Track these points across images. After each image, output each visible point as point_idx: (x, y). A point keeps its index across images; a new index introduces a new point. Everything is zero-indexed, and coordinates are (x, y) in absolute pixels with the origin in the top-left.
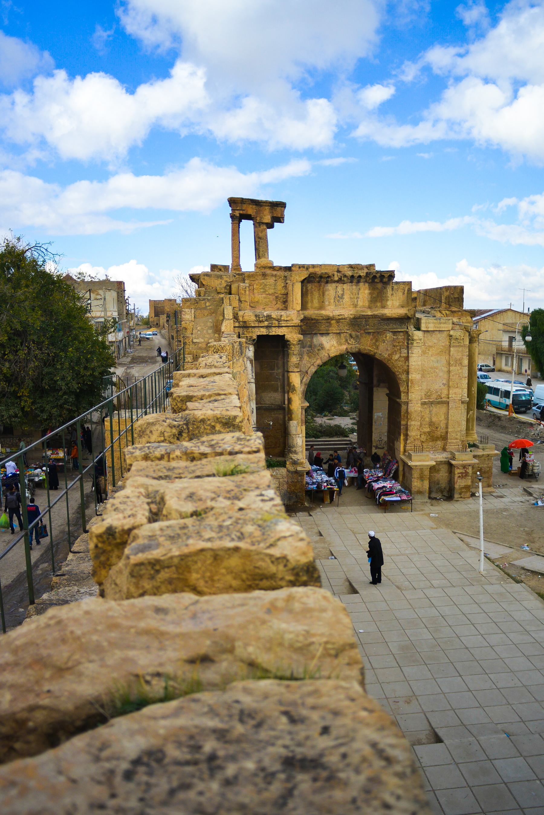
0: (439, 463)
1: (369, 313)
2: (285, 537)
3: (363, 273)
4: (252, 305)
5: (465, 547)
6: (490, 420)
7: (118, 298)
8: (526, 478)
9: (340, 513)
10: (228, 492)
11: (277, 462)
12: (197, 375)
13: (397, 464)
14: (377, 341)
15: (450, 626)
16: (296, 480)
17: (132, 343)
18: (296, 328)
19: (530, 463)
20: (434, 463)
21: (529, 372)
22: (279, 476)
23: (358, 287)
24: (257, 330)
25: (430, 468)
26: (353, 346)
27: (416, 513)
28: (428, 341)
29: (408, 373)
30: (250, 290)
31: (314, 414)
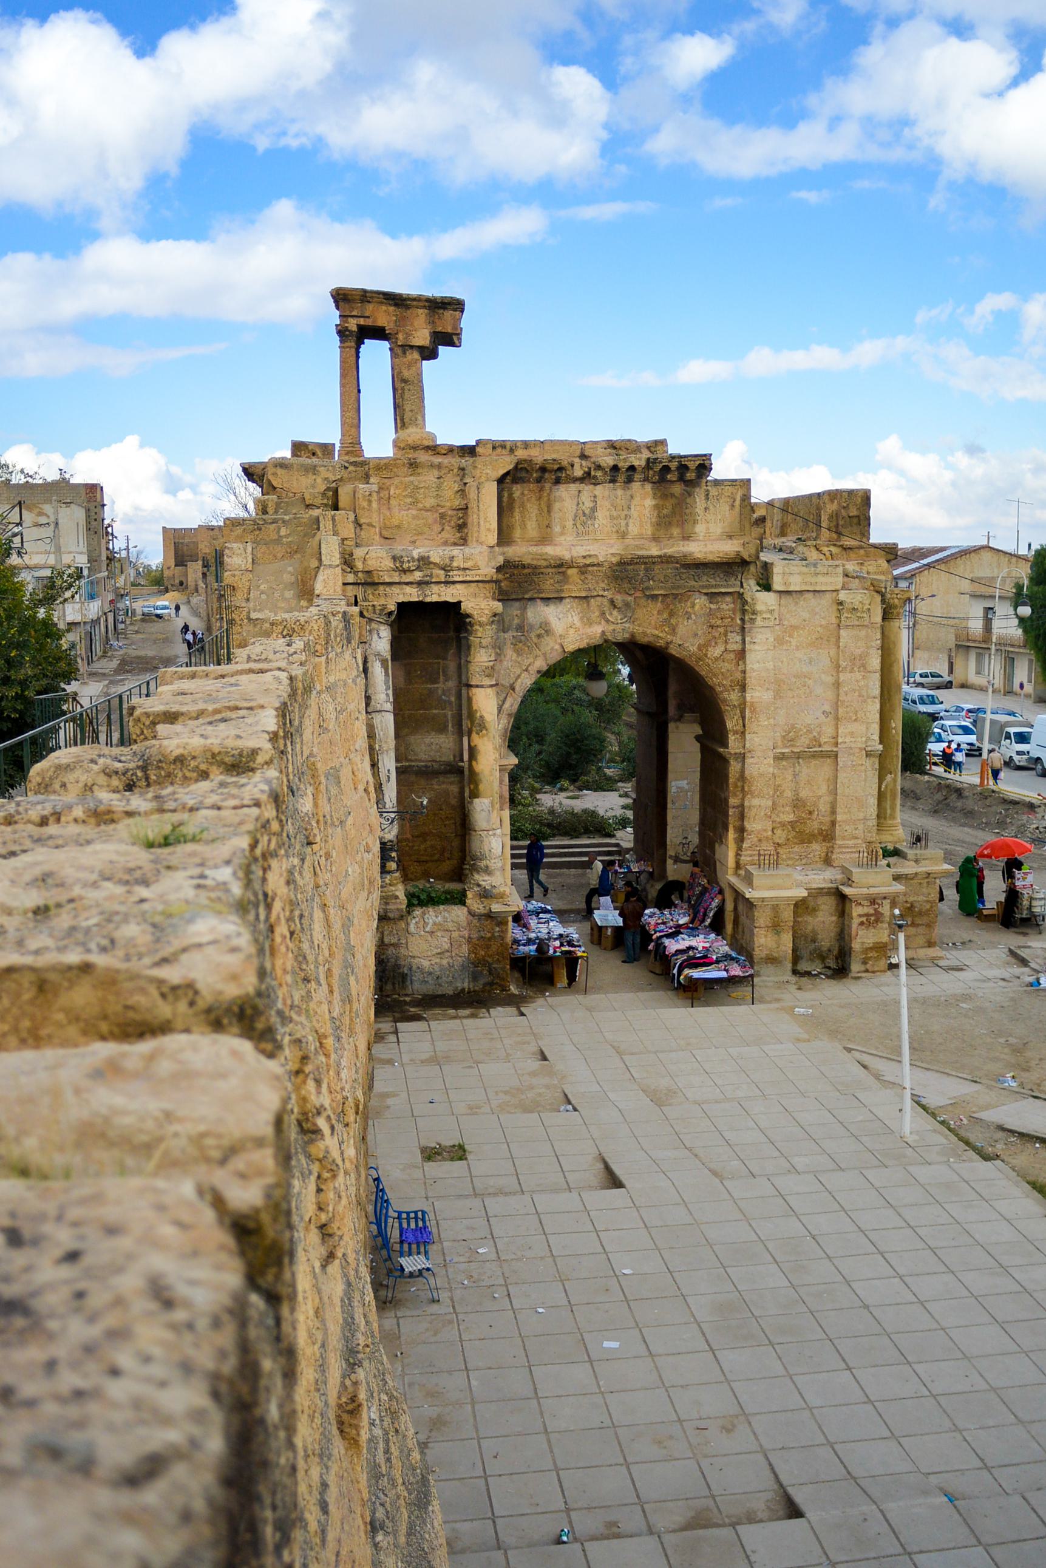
0: (821, 892)
1: (655, 551)
2: (199, 946)
3: (640, 459)
4: (386, 533)
5: (871, 1080)
6: (939, 796)
7: (88, 523)
8: (1015, 926)
9: (589, 1009)
10: (130, 871)
11: (446, 892)
12: (212, 676)
13: (720, 897)
14: (671, 614)
15: (829, 1257)
16: (489, 935)
17: (121, 626)
18: (487, 585)
19: (1024, 892)
20: (805, 894)
21: (1029, 688)
22: (450, 926)
23: (629, 493)
24: (398, 591)
25: (796, 905)
26: (618, 628)
27: (762, 1006)
28: (788, 616)
29: (743, 688)
30: (380, 499)
31: (537, 785)
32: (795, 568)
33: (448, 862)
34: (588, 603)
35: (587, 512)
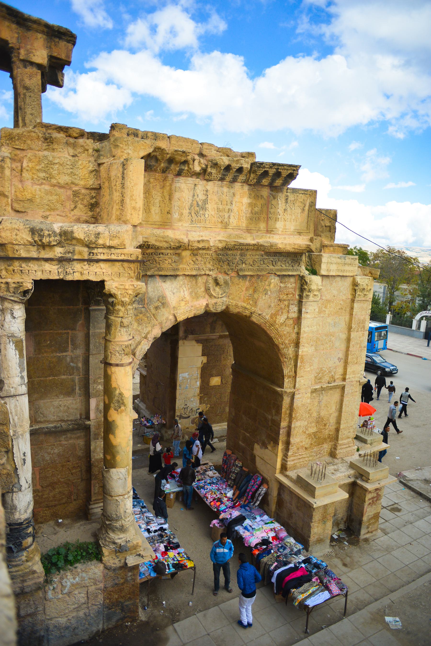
1: (249, 240)
4: (17, 206)
14: (255, 291)
16: (122, 581)
18: (132, 265)
23: (232, 191)
24: (36, 268)
32: (334, 259)
33: (74, 503)
34: (196, 280)
35: (200, 203)
